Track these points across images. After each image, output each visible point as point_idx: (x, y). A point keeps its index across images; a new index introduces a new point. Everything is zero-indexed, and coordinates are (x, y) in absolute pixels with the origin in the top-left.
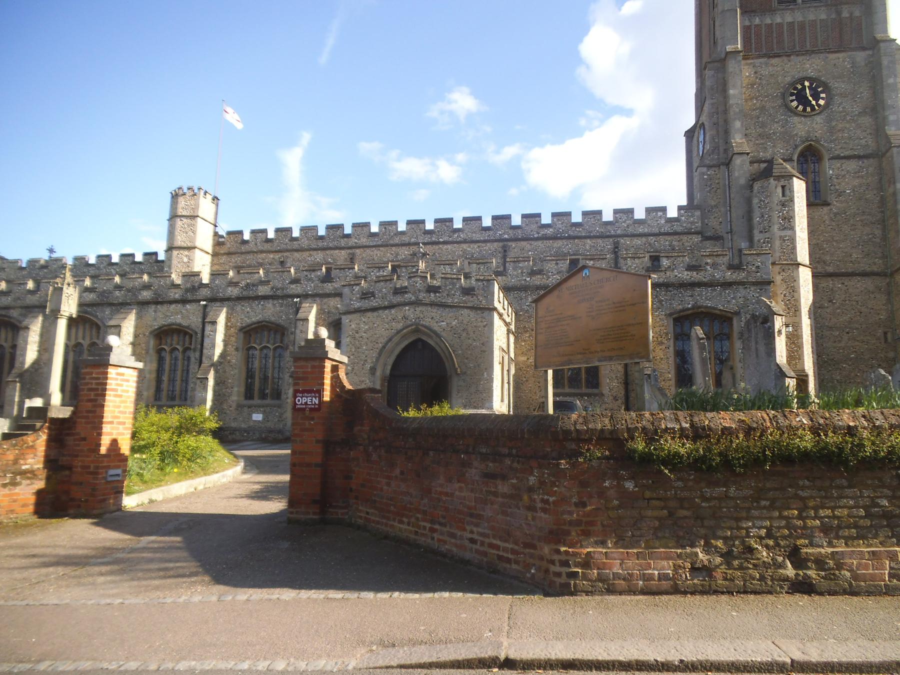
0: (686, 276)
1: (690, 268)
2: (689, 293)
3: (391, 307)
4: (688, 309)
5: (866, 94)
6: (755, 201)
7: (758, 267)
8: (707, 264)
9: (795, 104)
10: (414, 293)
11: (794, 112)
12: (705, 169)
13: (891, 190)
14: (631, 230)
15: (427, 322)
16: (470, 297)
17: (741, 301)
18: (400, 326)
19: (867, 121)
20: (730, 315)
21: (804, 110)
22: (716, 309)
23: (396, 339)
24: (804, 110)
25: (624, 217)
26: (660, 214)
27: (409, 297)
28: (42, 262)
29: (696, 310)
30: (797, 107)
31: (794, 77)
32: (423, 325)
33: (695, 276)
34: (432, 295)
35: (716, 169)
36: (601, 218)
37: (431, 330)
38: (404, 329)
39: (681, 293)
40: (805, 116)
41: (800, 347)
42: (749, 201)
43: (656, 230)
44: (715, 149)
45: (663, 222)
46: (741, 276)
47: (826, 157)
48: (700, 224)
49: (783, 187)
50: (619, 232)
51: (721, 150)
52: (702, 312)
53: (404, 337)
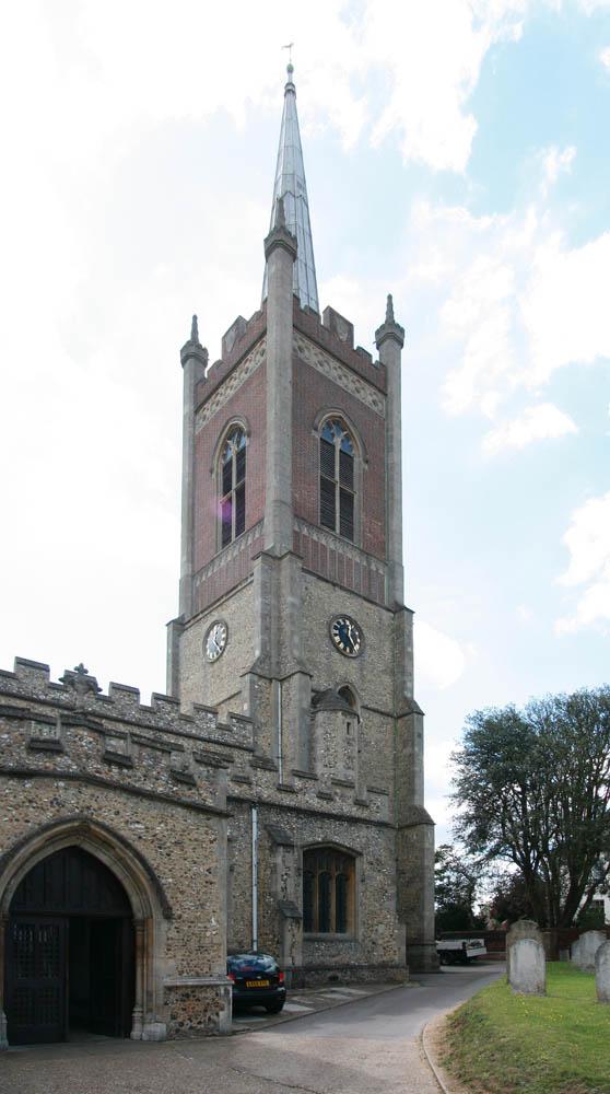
0: (316, 804)
1: (321, 796)
2: (319, 824)
3: (22, 774)
4: (319, 843)
5: (388, 654)
6: (319, 732)
7: (378, 807)
8: (336, 793)
9: (337, 639)
10: (77, 757)
11: (336, 646)
12: (256, 678)
13: (407, 751)
14: (175, 726)
15: (106, 817)
16: (185, 788)
17: (364, 840)
18: (47, 817)
19: (387, 680)
20: (354, 854)
21: (345, 649)
22: (343, 846)
23: (36, 842)
24: (345, 649)
25: (168, 707)
26: (210, 715)
27: (62, 763)
28: (165, 1033)
29: (350, 852)
30: (339, 643)
31: (337, 610)
32: (97, 824)
33: (325, 806)
34: (115, 770)
35: (267, 682)
36: (137, 701)
37: (116, 835)
38: (55, 825)
39: (311, 822)
40: (343, 654)
41: (56, 835)
42: (311, 729)
43: (204, 735)
44: (265, 657)
45: (213, 726)
46: (364, 814)
47: (359, 704)
48: (251, 740)
49: (349, 724)
50: (161, 724)
51: (274, 660)
52: (330, 848)
53: (51, 840)
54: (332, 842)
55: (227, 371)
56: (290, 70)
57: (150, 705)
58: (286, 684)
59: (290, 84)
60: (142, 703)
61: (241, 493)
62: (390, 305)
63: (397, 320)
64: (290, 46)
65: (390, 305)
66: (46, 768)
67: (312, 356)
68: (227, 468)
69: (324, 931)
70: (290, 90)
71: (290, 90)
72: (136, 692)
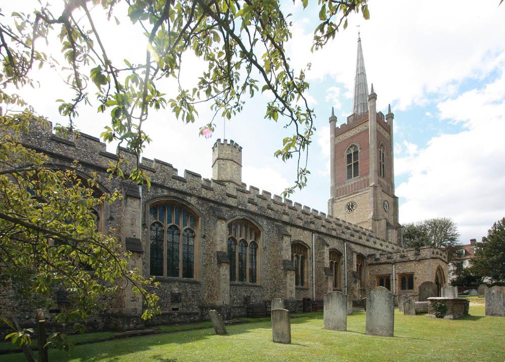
42: (387, 233)
52: (300, 244)
54: (301, 241)
55: (346, 128)
56: (359, 33)
57: (183, 176)
58: (379, 221)
59: (360, 38)
60: (179, 175)
61: (356, 164)
62: (333, 110)
63: (335, 115)
64: (359, 26)
65: (333, 110)
66: (96, 164)
67: (381, 130)
68: (349, 156)
69: (439, 296)
70: (359, 41)
71: (359, 41)
72: (258, 190)
